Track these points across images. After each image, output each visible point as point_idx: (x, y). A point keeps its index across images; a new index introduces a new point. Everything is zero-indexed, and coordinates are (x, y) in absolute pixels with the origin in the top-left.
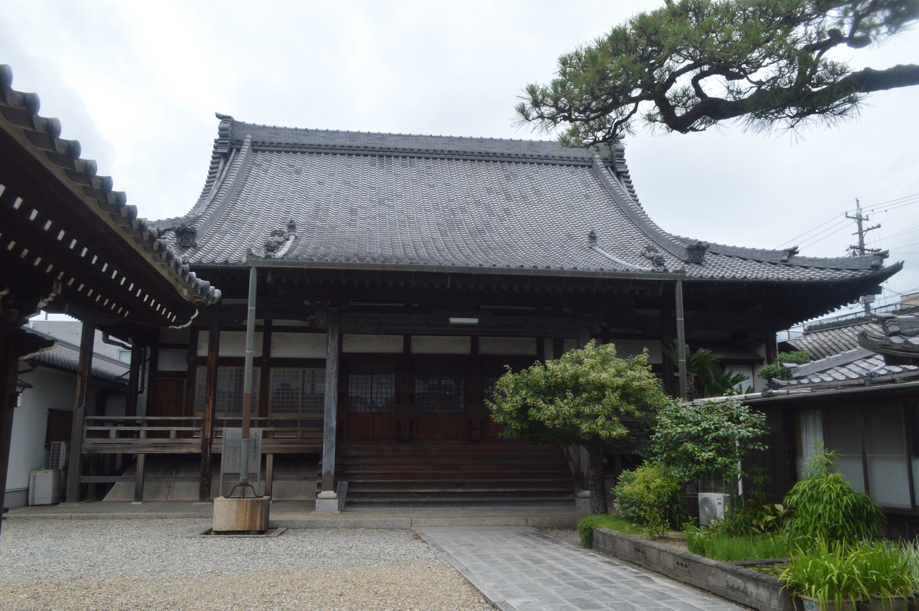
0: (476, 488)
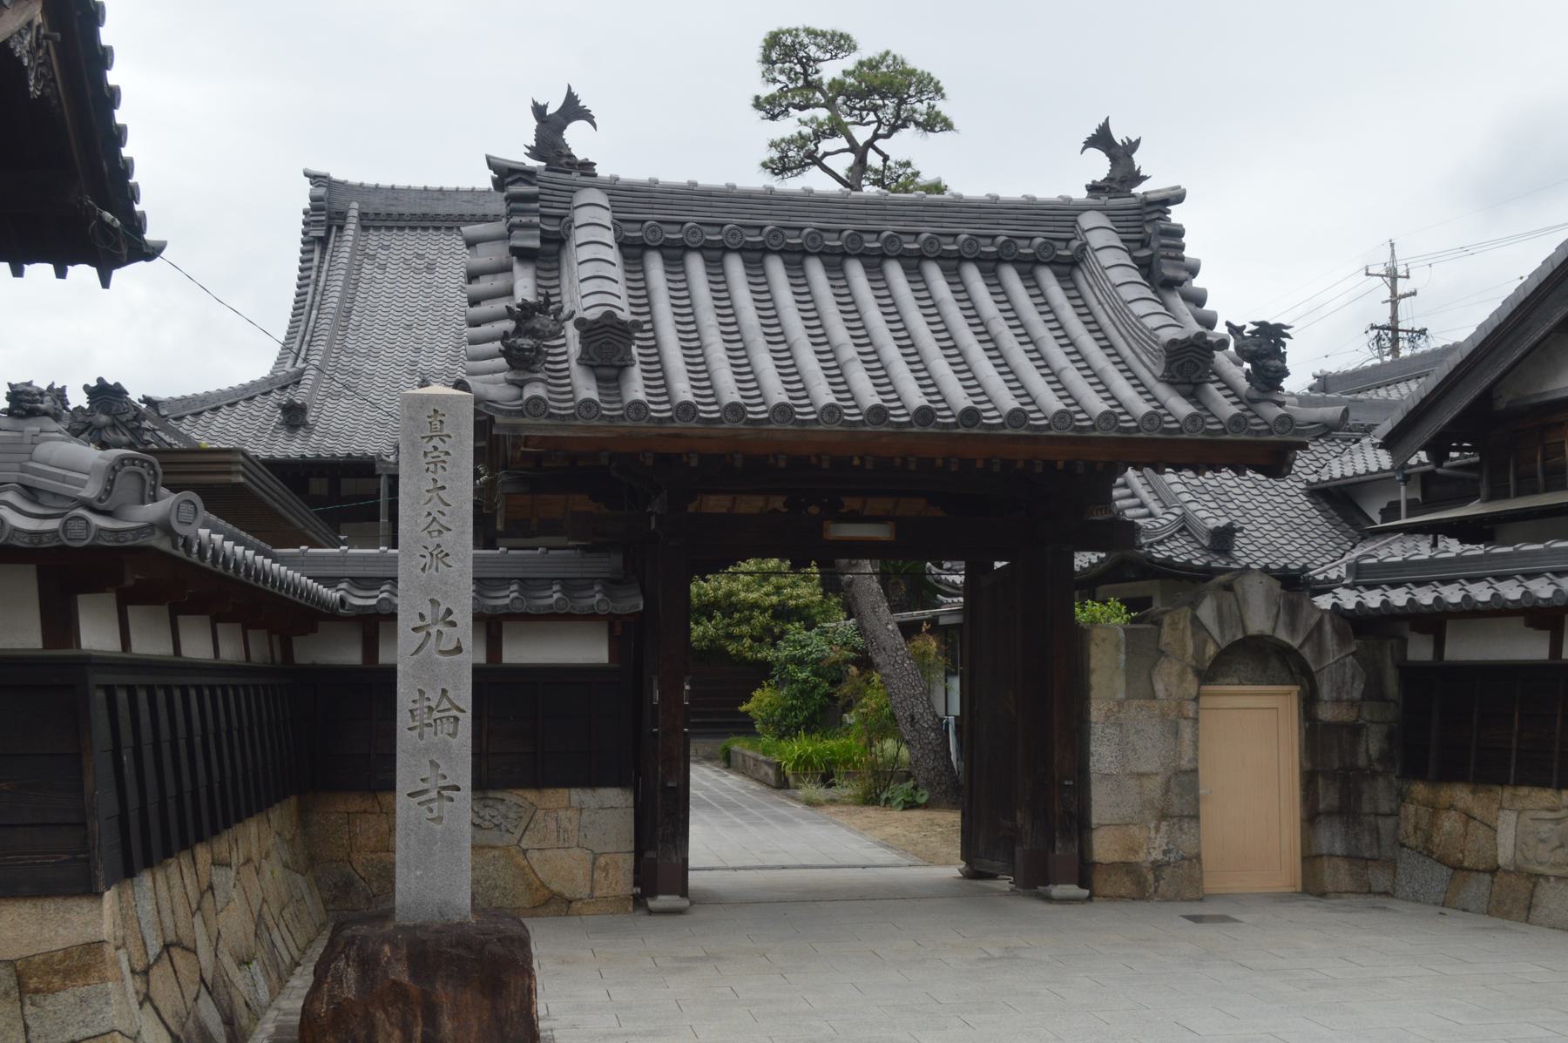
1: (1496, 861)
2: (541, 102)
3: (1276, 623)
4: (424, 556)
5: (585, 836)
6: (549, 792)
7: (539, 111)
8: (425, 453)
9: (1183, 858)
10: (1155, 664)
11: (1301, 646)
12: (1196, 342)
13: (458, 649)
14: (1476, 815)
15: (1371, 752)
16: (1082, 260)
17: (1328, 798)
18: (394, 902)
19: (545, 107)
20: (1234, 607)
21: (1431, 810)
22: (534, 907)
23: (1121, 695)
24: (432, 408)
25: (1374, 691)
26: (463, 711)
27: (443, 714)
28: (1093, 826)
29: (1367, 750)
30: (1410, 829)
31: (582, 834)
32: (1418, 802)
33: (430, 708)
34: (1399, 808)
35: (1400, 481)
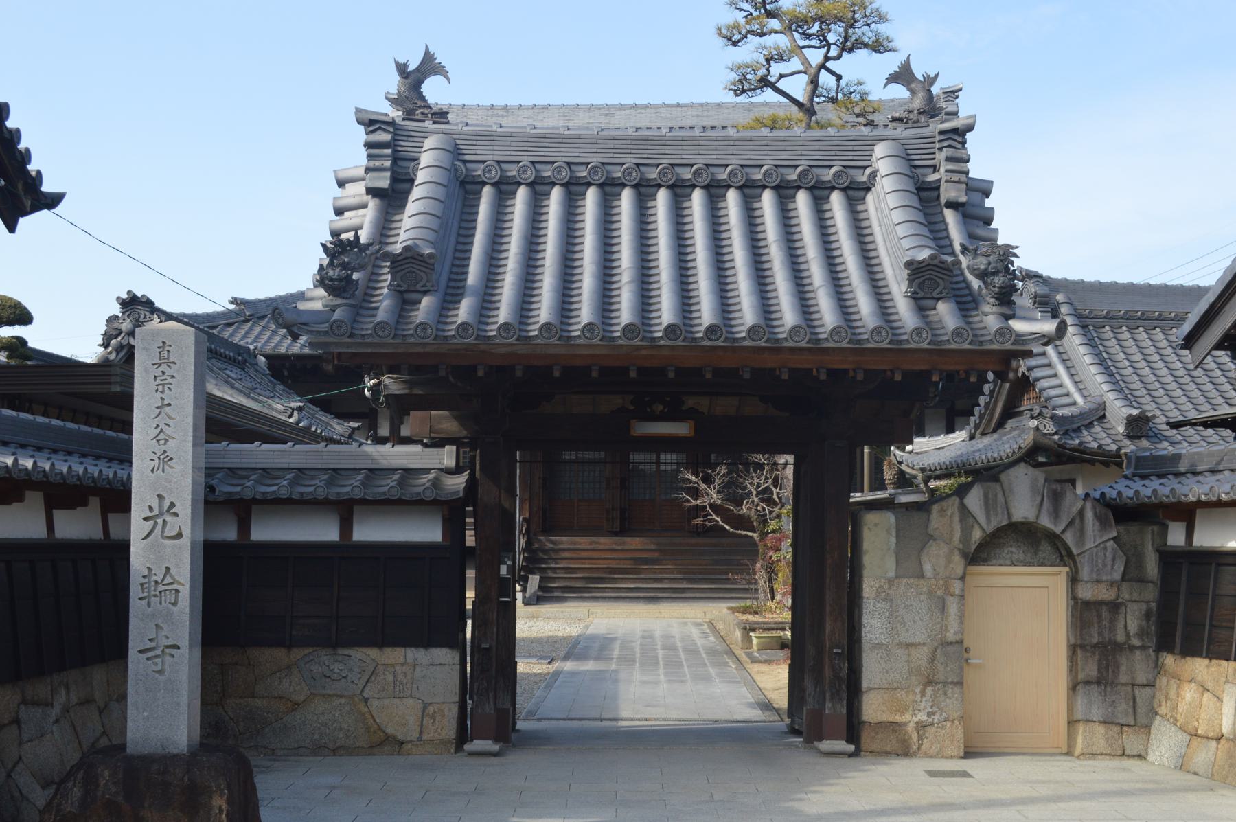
1: (1221, 730)
2: (402, 61)
3: (1040, 511)
4: (152, 460)
5: (418, 688)
6: (388, 650)
7: (402, 69)
8: (155, 377)
10: (923, 547)
11: (1063, 532)
12: (931, 262)
13: (179, 536)
16: (874, 186)
17: (1090, 669)
18: (126, 738)
19: (405, 65)
20: (1000, 495)
21: (1178, 682)
22: (372, 747)
23: (892, 574)
24: (162, 340)
25: (1133, 574)
26: (183, 585)
27: (166, 587)
28: (864, 690)
29: (1126, 627)
31: (415, 686)
33: (156, 582)
34: (1155, 679)
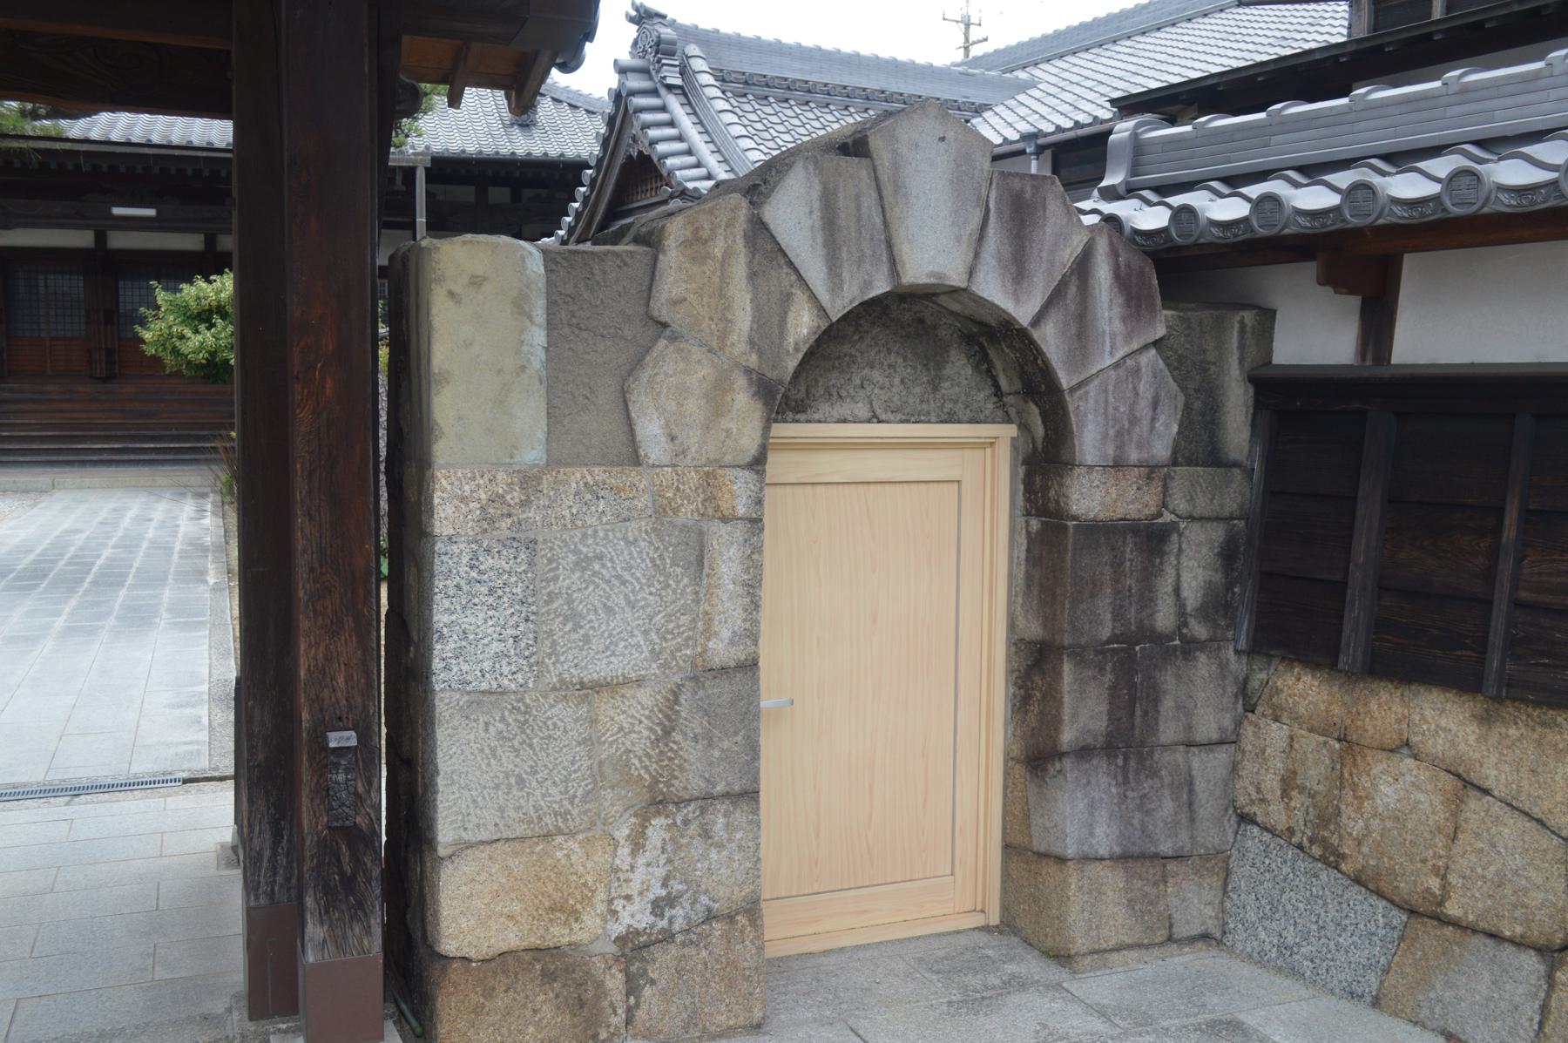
0: (172, 442)
3: (977, 255)
9: (710, 917)
10: (638, 362)
11: (1037, 321)
14: (1490, 784)
15: (1185, 594)
20: (869, 201)
23: (533, 454)
29: (1177, 590)
30: (1271, 783)
32: (1297, 718)
34: (1238, 724)
35: (1031, 154)
